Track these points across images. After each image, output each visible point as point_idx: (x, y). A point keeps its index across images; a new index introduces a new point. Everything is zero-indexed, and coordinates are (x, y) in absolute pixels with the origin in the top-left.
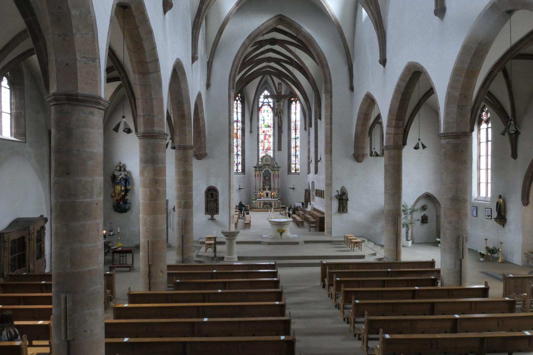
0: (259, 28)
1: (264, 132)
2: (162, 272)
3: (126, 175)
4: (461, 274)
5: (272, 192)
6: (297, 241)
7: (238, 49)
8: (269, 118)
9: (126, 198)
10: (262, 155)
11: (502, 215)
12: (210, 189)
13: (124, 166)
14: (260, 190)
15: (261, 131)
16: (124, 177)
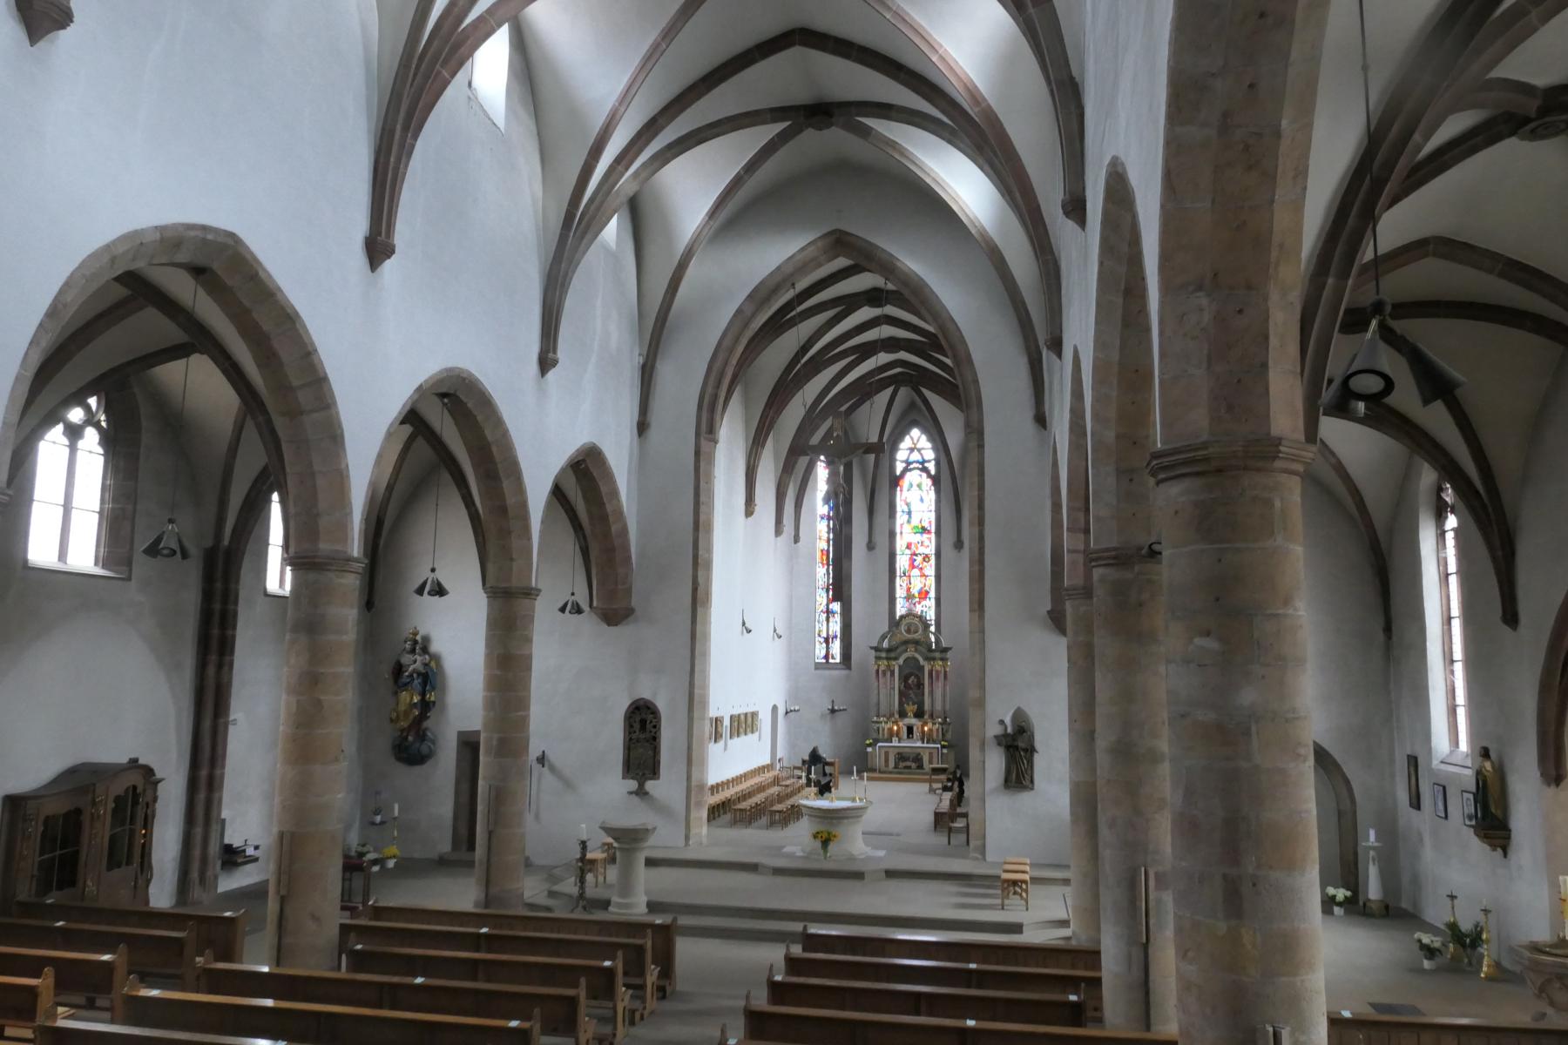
0: (778, 268)
1: (909, 546)
2: (315, 918)
3: (426, 665)
4: (1147, 993)
5: (925, 724)
6: (863, 869)
7: (719, 334)
8: (924, 506)
9: (426, 724)
10: (901, 609)
11: (1494, 817)
12: (637, 708)
13: (426, 640)
14: (892, 715)
15: (900, 544)
16: (421, 669)
